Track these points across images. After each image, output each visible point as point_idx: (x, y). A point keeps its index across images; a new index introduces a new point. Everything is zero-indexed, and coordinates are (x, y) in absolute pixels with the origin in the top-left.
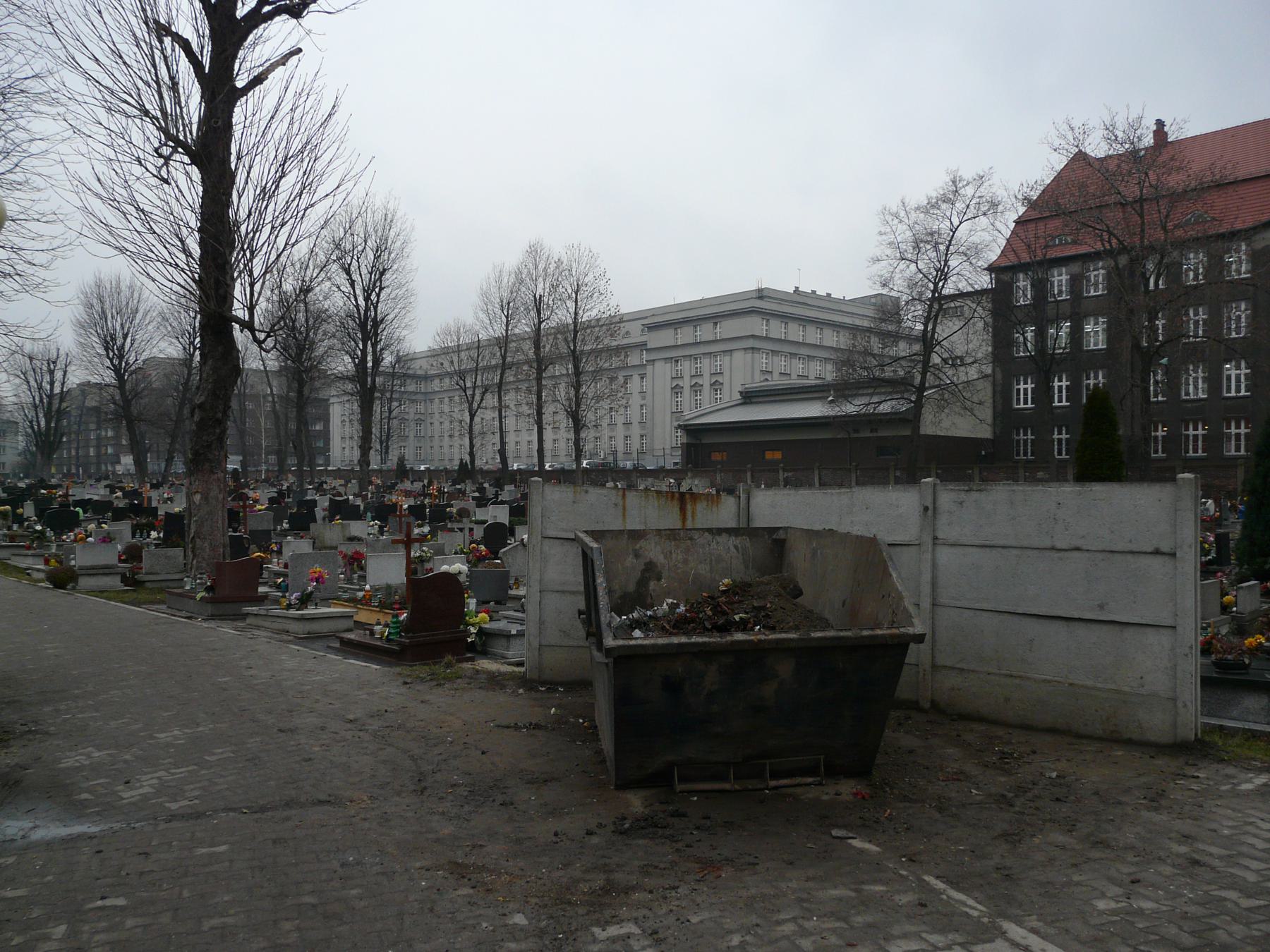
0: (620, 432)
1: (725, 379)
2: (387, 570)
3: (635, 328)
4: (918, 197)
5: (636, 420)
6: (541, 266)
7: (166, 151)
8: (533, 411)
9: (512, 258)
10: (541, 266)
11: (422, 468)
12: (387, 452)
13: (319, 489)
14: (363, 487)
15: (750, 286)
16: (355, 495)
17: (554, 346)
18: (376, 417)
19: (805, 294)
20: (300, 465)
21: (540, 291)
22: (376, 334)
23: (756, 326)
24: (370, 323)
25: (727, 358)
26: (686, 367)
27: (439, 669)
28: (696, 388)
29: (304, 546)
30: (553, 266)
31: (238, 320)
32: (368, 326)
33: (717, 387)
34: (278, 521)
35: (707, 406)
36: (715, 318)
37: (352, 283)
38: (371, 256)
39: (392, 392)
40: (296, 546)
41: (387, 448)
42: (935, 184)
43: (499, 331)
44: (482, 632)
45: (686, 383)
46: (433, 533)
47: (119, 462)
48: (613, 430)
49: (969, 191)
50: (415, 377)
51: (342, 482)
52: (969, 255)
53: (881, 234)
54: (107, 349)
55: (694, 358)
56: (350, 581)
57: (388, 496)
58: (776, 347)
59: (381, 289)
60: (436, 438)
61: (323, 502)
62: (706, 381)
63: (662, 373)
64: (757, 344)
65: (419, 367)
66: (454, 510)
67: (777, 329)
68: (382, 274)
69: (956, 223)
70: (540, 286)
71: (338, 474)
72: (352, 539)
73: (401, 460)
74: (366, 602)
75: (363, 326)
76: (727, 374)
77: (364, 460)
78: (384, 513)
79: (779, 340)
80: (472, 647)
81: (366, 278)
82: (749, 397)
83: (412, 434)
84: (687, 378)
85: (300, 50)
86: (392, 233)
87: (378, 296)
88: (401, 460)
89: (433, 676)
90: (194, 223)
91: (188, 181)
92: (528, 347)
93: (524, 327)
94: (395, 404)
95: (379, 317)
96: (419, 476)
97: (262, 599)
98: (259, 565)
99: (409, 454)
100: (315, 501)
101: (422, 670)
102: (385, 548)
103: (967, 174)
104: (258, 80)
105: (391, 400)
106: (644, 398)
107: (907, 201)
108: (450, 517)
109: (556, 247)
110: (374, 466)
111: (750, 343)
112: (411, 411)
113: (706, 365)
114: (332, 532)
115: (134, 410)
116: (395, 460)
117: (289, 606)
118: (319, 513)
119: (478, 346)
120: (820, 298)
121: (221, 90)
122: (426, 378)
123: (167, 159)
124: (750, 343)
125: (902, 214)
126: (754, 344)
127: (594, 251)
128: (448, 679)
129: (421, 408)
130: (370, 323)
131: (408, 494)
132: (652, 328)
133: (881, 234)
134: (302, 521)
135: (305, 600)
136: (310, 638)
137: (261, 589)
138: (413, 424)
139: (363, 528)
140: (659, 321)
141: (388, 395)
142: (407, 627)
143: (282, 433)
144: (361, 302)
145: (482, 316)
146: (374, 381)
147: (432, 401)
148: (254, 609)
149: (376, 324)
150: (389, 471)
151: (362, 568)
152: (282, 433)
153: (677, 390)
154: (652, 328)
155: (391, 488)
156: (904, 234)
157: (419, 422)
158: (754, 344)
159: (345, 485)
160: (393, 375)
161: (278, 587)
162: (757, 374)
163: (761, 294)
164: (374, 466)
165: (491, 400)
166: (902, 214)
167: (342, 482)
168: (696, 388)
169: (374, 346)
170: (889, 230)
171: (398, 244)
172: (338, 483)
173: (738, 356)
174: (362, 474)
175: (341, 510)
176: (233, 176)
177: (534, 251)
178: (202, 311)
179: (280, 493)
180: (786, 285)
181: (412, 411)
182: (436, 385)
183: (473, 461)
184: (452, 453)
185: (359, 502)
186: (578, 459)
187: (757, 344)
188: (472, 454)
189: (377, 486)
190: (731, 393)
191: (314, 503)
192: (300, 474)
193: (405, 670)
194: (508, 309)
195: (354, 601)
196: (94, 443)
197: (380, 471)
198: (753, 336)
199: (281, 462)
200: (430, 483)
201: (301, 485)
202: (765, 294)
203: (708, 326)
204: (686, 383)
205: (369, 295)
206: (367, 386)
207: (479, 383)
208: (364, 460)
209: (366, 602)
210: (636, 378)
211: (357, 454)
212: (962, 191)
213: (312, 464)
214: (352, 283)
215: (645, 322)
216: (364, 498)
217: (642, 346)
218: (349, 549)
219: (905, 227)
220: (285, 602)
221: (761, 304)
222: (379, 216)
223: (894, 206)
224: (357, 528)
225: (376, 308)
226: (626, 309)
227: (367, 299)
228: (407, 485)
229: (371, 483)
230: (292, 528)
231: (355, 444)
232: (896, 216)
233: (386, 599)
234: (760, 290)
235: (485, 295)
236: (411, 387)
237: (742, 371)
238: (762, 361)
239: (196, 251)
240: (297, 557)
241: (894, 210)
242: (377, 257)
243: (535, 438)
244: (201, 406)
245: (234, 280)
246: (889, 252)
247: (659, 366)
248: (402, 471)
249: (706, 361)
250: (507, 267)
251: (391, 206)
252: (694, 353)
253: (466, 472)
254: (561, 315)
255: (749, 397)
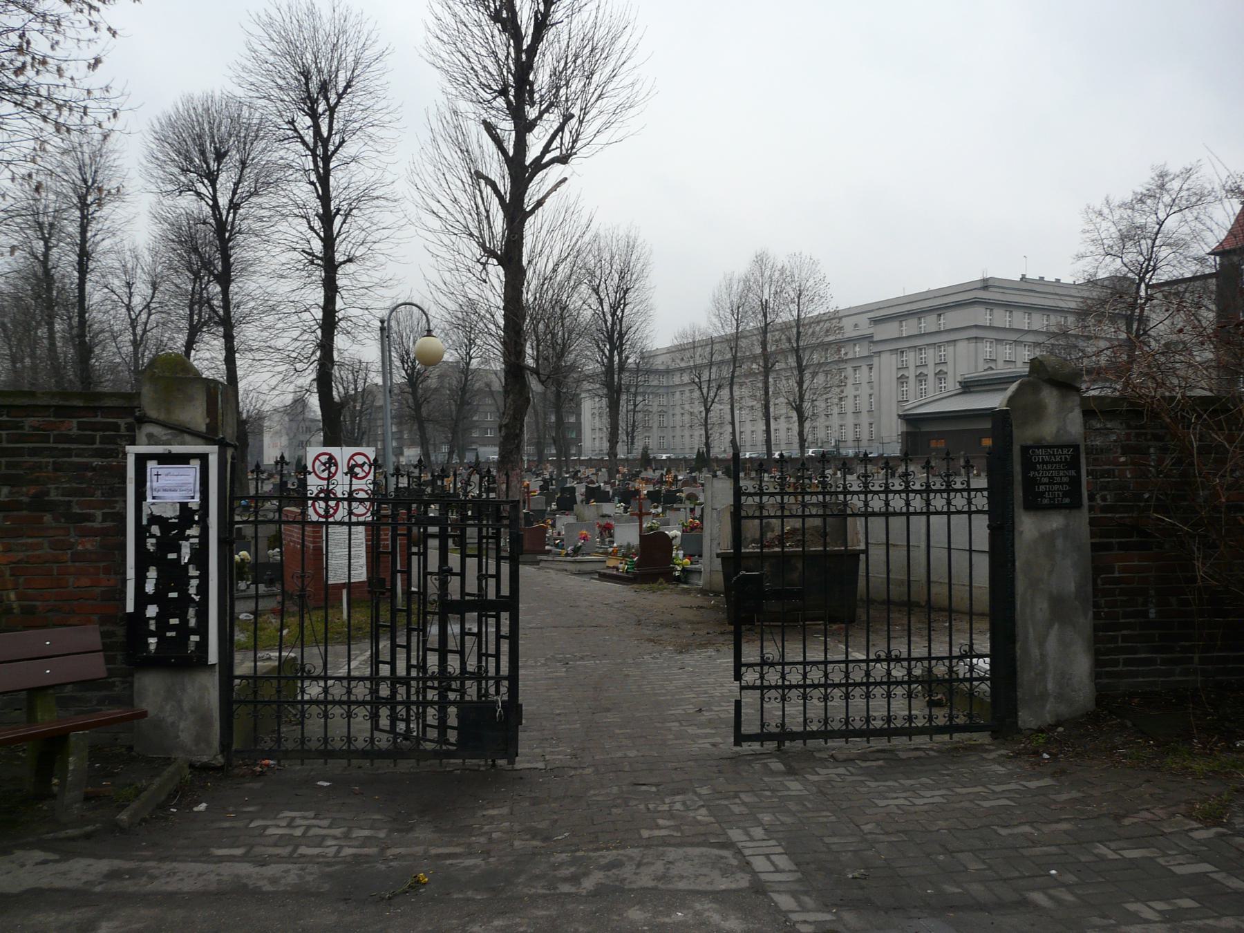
0: (850, 420)
1: (949, 368)
2: (628, 535)
3: (863, 321)
4: (1126, 194)
5: (864, 408)
6: (767, 274)
7: (483, 260)
8: (758, 406)
9: (741, 266)
10: (767, 274)
11: (664, 457)
12: (633, 443)
13: (575, 476)
14: (611, 475)
15: (973, 275)
16: (605, 483)
17: (778, 346)
18: (623, 409)
19: (1032, 281)
20: (558, 455)
21: (766, 297)
22: (622, 344)
23: (982, 316)
24: (616, 336)
25: (951, 349)
26: (911, 358)
27: (655, 586)
28: (921, 378)
29: (570, 519)
30: (777, 274)
31: (529, 368)
32: (614, 335)
33: (940, 375)
34: (548, 503)
35: (931, 394)
36: (939, 310)
37: (601, 302)
38: (616, 277)
39: (637, 386)
40: (563, 521)
41: (633, 438)
42: (1142, 180)
43: (730, 330)
44: (684, 570)
45: (911, 373)
46: (663, 512)
47: (402, 454)
48: (842, 419)
49: (1175, 185)
50: (657, 372)
51: (594, 470)
52: (1177, 245)
53: (1084, 231)
54: (403, 362)
55: (919, 349)
56: (603, 542)
57: (632, 484)
58: (1001, 336)
59: (625, 305)
60: (673, 430)
61: (581, 489)
62: (930, 371)
63: (888, 364)
64: (980, 333)
65: (659, 363)
66: (683, 495)
67: (1001, 318)
68: (625, 293)
69: (1162, 216)
70: (766, 291)
71: (589, 463)
72: (604, 516)
73: (646, 449)
74: (614, 554)
75: (610, 338)
76: (950, 364)
77: (612, 452)
78: (627, 496)
79: (1004, 329)
80: (678, 579)
81: (612, 295)
82: (968, 387)
83: (655, 426)
84: (912, 368)
85: (565, 179)
86: (634, 257)
87: (623, 311)
88: (646, 449)
89: (651, 589)
90: (502, 305)
91: (496, 273)
92: (756, 339)
93: (753, 324)
94: (639, 398)
95: (624, 329)
96: (661, 464)
97: (549, 552)
98: (544, 530)
99: (653, 444)
100: (574, 488)
101: (646, 586)
102: (627, 521)
103: (1174, 168)
104: (540, 203)
105: (635, 395)
106: (872, 388)
107: (1111, 198)
108: (680, 500)
109: (780, 256)
110: (621, 456)
111: (974, 333)
112: (655, 404)
113: (930, 355)
114: (590, 511)
115: (424, 411)
116: (640, 451)
117: (567, 555)
118: (579, 498)
119: (711, 342)
120: (1049, 284)
121: (516, 214)
122: (668, 372)
123: (484, 264)
124: (974, 333)
125: (1106, 211)
126: (977, 333)
127: (815, 258)
128: (659, 589)
129: (663, 400)
130: (616, 336)
131: (647, 481)
132: (876, 321)
133: (1084, 231)
134: (567, 503)
135: (577, 551)
136: (580, 573)
137: (547, 547)
138: (656, 417)
139: (610, 509)
140: (884, 314)
141: (633, 390)
142: (638, 565)
143: (541, 427)
144: (609, 318)
145: (715, 320)
146: (620, 379)
147: (673, 394)
148: (545, 558)
149: (621, 336)
150: (635, 460)
151: (611, 536)
152: (541, 427)
153: (902, 380)
154: (876, 321)
155: (635, 476)
156: (1109, 231)
157: (662, 413)
158: (977, 333)
159: (596, 474)
160: (637, 370)
161: (557, 546)
162: (981, 361)
163: (986, 284)
164: (621, 456)
165: (725, 393)
166: (1106, 211)
167: (594, 470)
168: (921, 378)
169: (620, 354)
170: (1092, 227)
171: (639, 266)
172: (590, 472)
173: (962, 346)
174: (611, 463)
175: (595, 495)
176: (525, 271)
177: (760, 260)
178: (505, 362)
179: (544, 480)
180: (1012, 274)
181: (656, 404)
182: (676, 380)
183: (708, 451)
184: (689, 443)
185: (608, 488)
186: (802, 446)
187: (980, 333)
188: (707, 445)
189: (624, 475)
190: (952, 385)
191: (573, 490)
192: (558, 464)
193: (636, 586)
194: (738, 311)
195: (606, 553)
196: (380, 438)
197: (627, 460)
198: (976, 326)
199: (540, 453)
200: (669, 472)
201: (560, 474)
202: (990, 283)
203: (932, 318)
204: (911, 373)
205: (615, 311)
206: (614, 385)
207: (713, 377)
208: (612, 452)
209: (614, 554)
210: (865, 369)
211: (606, 445)
212: (1168, 186)
213: (567, 455)
214: (601, 302)
215: (871, 315)
216: (613, 485)
217: (869, 338)
218: (603, 522)
219: (1110, 224)
220: (564, 552)
221: (985, 294)
222: (622, 244)
223: (1098, 204)
224: (607, 508)
225: (621, 321)
226: (843, 306)
227: (613, 314)
228: (649, 474)
229: (618, 472)
230: (559, 509)
231: (605, 435)
232: (1101, 214)
233: (626, 553)
234: (985, 280)
235: (717, 302)
236: (654, 382)
237: (966, 360)
238: (987, 349)
239: (501, 322)
240: (568, 526)
241: (1098, 208)
242: (621, 278)
243: (762, 426)
244: (505, 426)
245: (526, 340)
246: (1093, 248)
247: (885, 357)
248: (646, 461)
249: (931, 352)
250: (736, 275)
251: (632, 234)
252: (917, 342)
253: (703, 461)
254: (786, 316)
255: (968, 387)
